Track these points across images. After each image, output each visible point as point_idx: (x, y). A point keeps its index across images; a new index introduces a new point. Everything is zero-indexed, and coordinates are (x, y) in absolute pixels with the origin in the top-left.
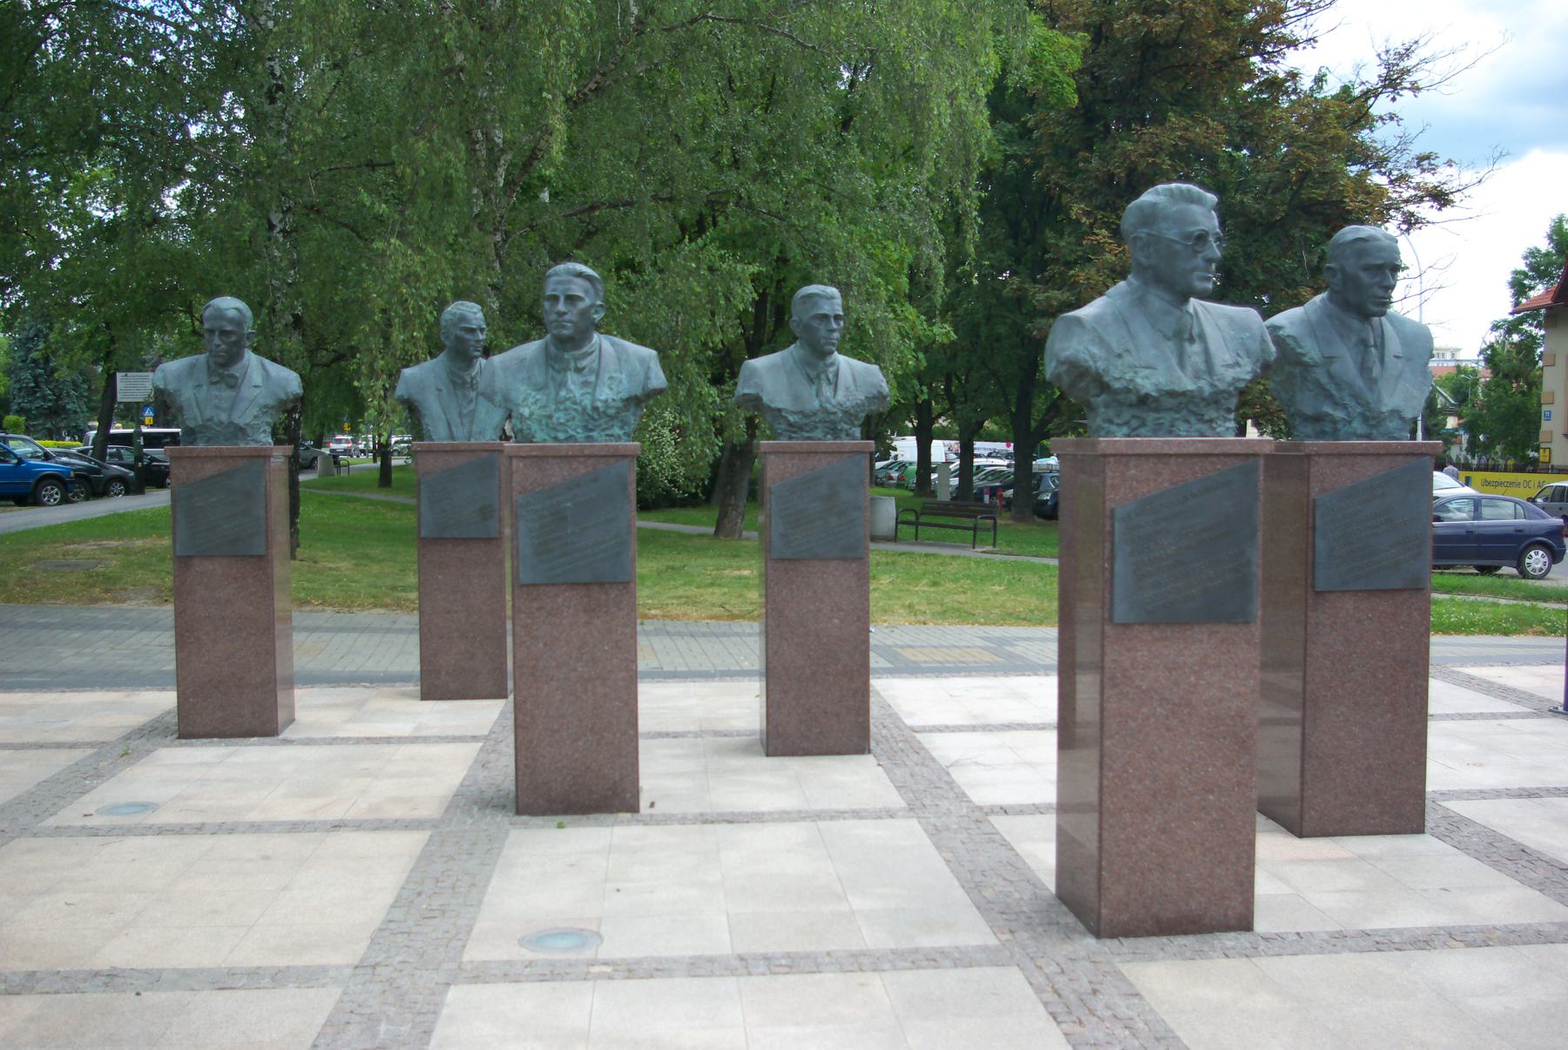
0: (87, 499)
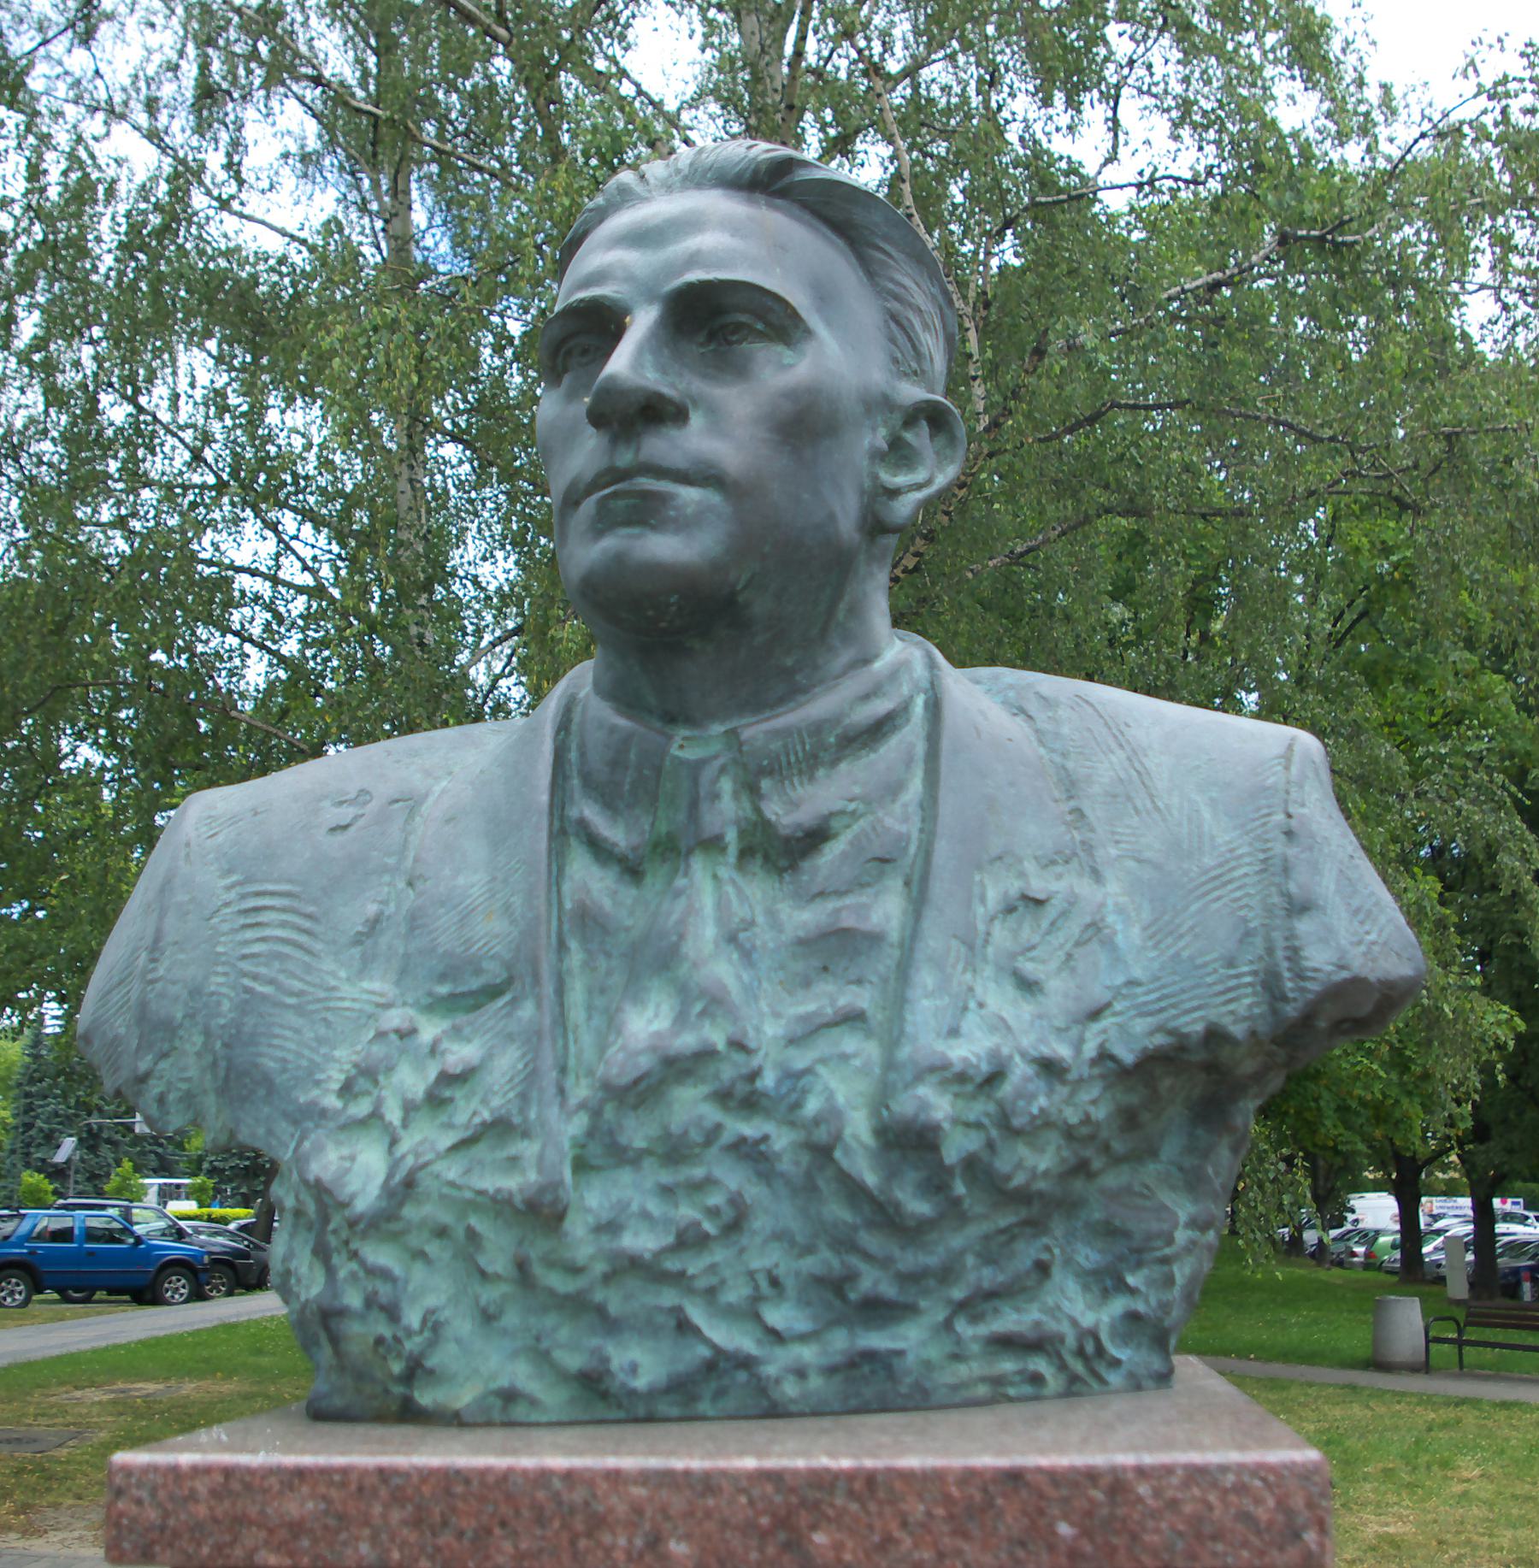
0: (230, 1294)
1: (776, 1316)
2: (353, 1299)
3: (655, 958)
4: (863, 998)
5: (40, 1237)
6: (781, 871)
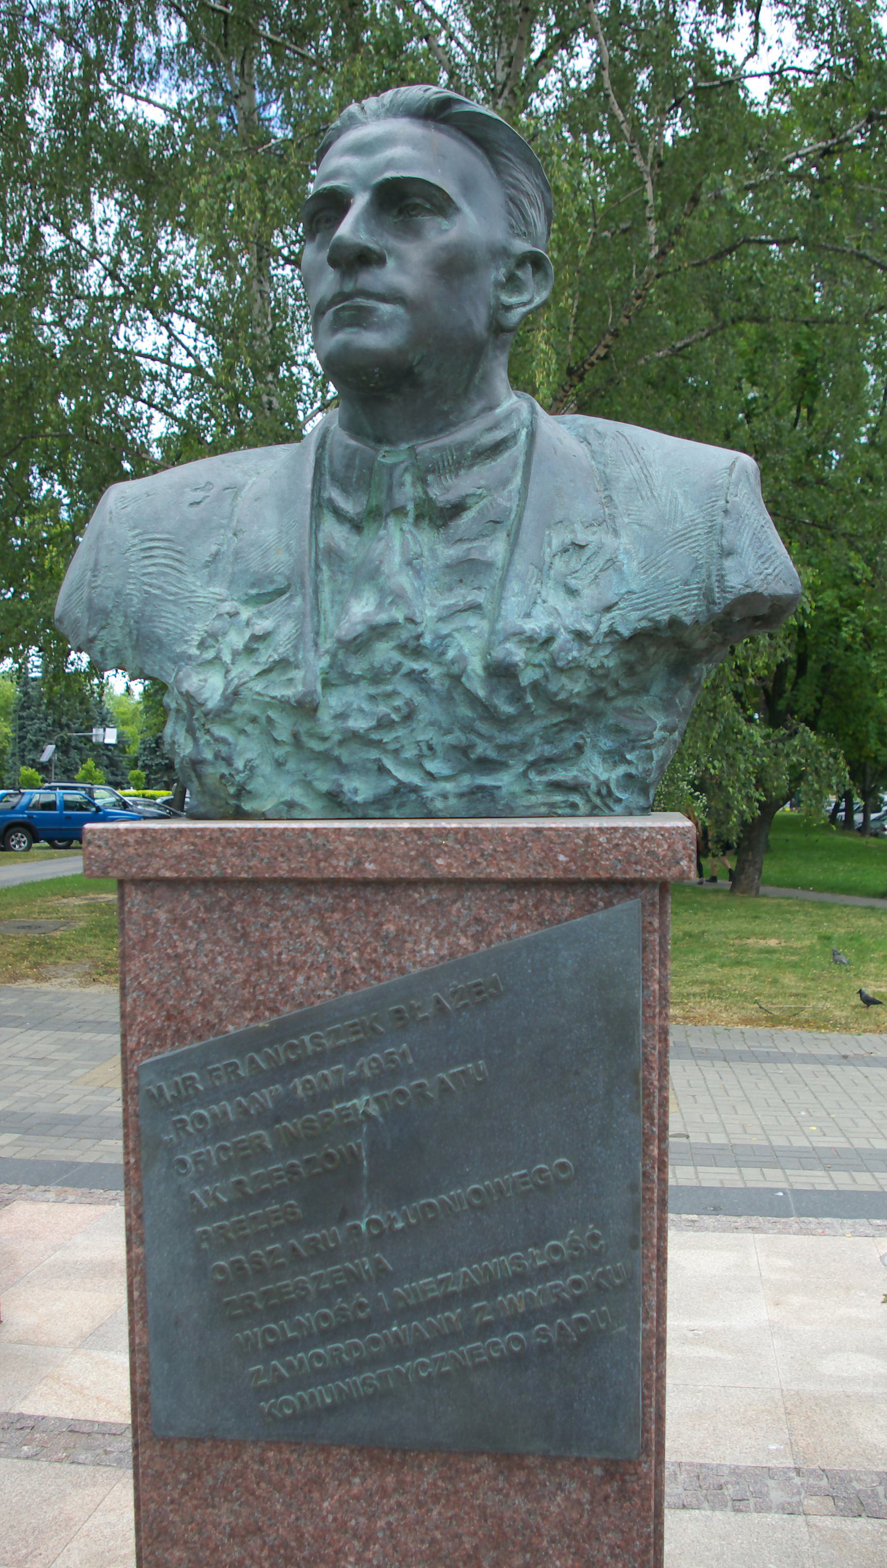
1: (432, 766)
2: (208, 755)
3: (370, 574)
4: (480, 597)
5: (34, 807)
6: (438, 527)
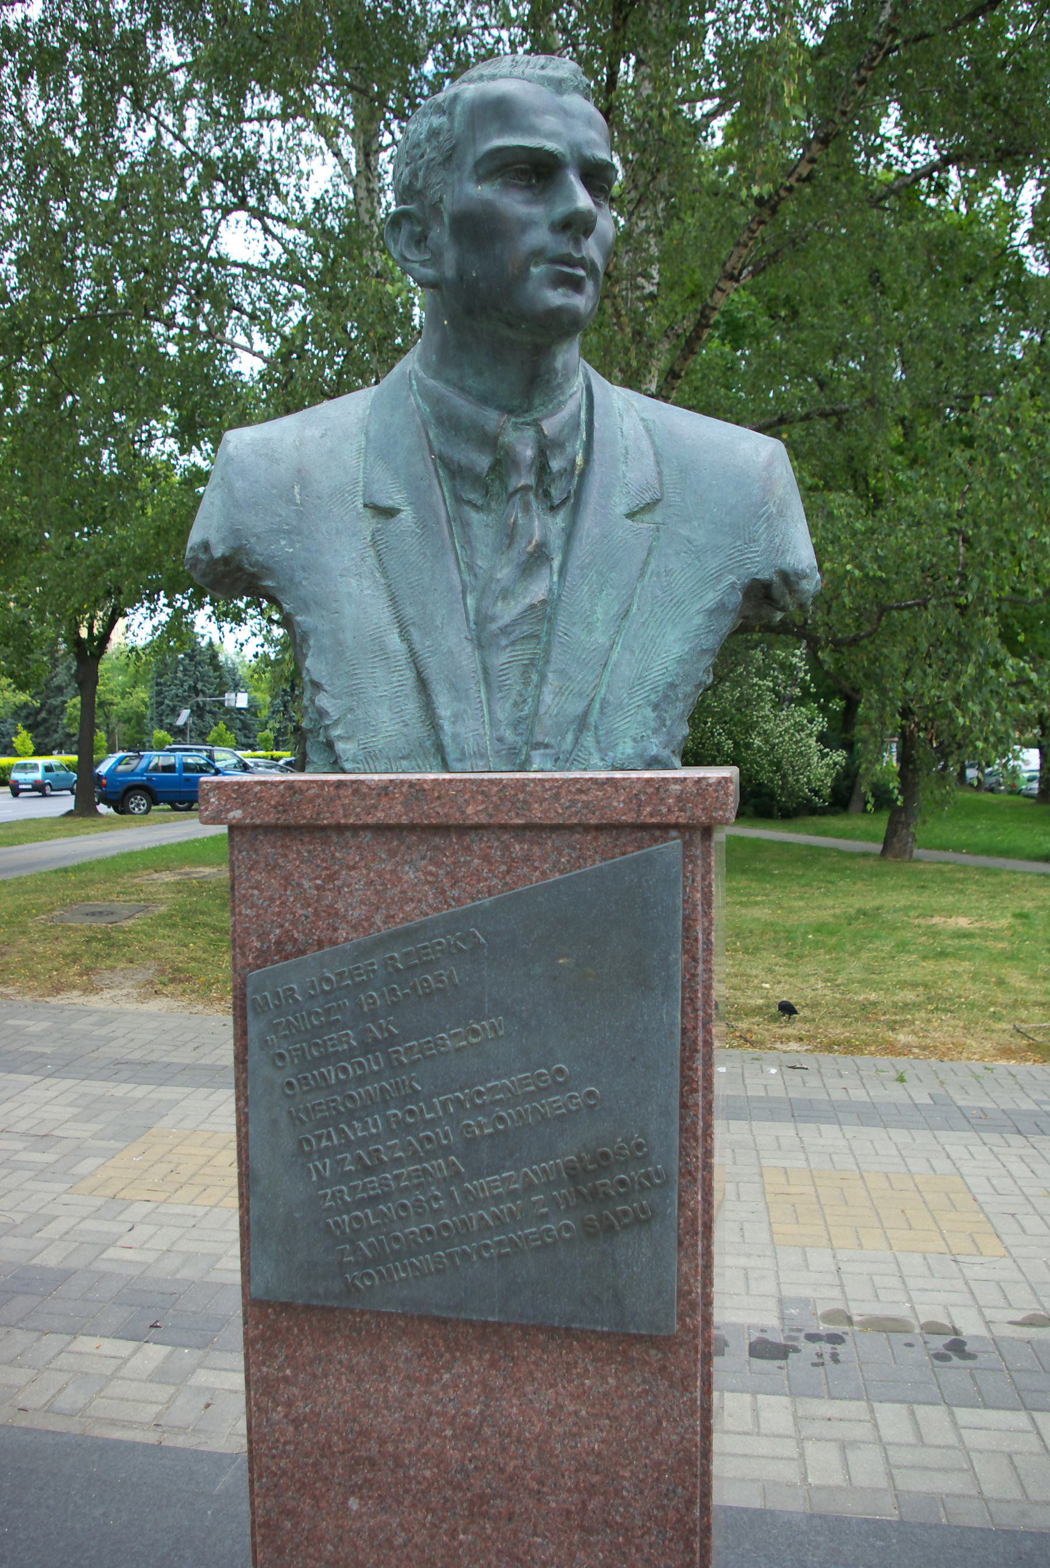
5: (156, 769)
